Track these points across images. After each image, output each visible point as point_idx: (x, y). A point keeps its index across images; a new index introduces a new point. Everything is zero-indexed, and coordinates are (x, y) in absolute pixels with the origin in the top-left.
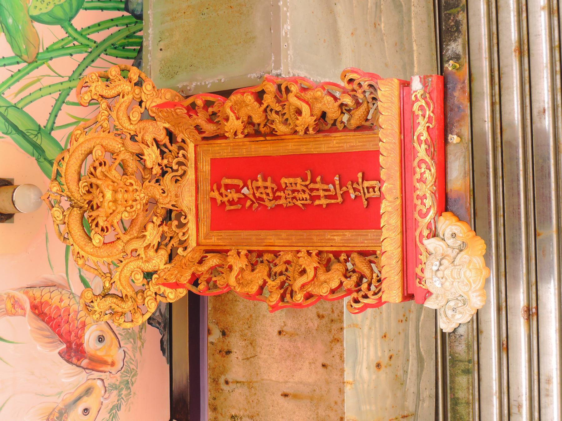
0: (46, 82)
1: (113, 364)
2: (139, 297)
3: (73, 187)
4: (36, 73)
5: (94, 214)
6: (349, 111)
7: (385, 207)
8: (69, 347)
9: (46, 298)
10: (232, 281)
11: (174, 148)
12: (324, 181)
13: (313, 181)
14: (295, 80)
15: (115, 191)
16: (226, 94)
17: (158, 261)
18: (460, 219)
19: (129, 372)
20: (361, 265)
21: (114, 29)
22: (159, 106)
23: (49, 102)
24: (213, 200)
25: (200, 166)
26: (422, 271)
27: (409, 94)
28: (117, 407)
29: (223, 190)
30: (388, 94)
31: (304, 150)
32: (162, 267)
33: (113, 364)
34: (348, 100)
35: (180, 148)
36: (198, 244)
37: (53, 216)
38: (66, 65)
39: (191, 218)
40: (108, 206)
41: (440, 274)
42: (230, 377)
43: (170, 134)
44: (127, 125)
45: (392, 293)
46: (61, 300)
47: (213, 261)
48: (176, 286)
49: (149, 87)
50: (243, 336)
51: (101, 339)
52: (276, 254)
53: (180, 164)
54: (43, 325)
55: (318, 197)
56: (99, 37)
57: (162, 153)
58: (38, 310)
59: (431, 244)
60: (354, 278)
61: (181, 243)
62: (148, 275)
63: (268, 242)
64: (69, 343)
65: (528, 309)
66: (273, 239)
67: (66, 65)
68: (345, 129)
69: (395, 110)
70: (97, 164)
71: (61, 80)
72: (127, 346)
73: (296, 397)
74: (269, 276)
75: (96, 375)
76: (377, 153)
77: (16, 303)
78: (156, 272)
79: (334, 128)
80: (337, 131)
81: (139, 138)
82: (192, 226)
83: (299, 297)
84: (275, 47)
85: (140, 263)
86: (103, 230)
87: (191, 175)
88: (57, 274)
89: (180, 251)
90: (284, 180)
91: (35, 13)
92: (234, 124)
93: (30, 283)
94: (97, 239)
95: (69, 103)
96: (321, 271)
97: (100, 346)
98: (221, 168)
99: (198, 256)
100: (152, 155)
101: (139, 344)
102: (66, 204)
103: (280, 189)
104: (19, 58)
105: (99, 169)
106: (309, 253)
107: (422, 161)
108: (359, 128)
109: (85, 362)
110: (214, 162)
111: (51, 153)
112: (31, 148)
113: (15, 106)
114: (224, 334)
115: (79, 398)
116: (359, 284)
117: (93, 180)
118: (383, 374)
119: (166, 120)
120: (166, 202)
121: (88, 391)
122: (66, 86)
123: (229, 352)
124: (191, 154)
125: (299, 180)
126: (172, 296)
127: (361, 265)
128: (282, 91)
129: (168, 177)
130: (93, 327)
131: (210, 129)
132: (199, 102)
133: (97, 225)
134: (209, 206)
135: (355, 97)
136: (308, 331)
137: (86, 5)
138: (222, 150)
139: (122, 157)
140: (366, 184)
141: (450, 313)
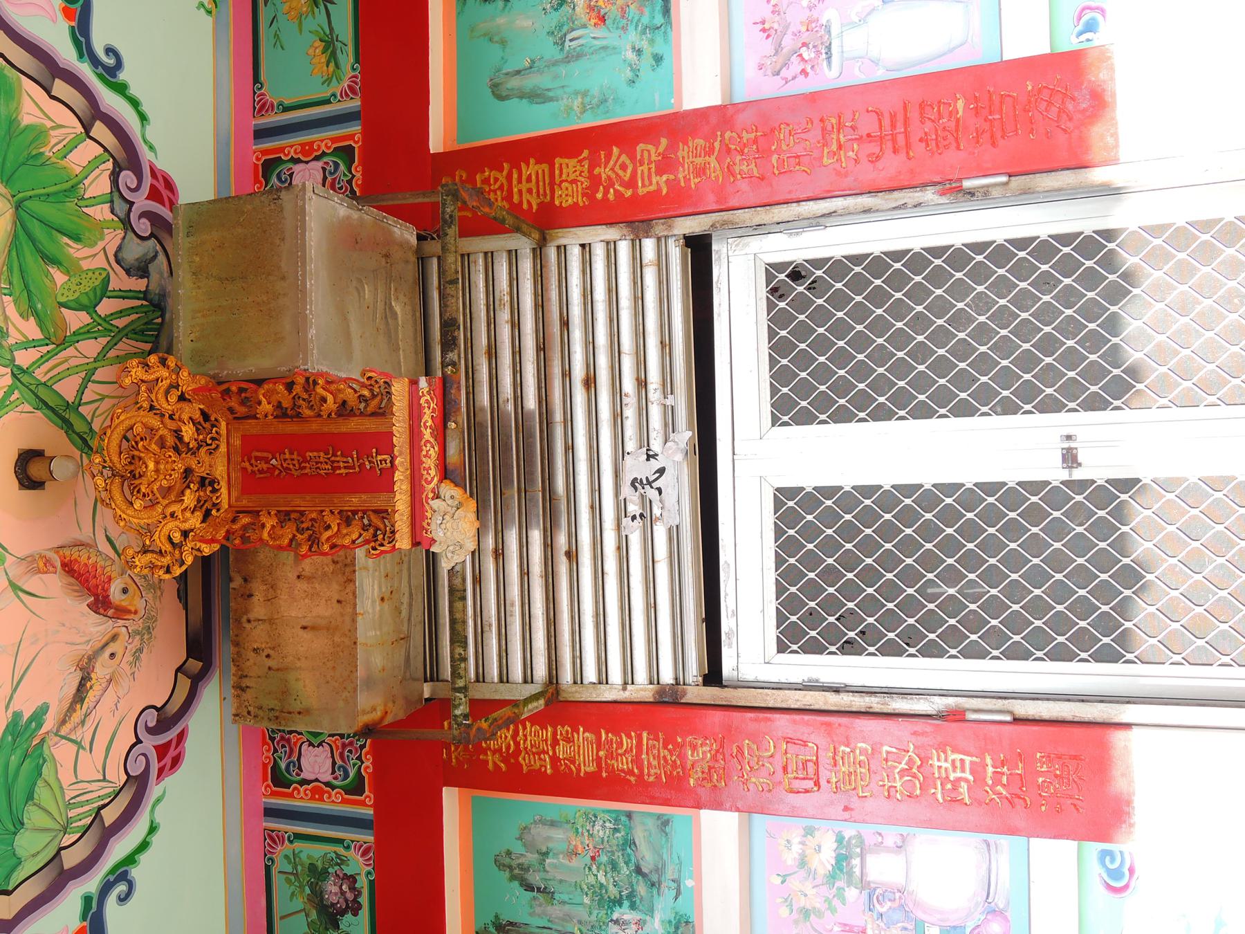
0: (73, 362)
1: (136, 612)
2: (177, 552)
3: (115, 459)
4: (63, 354)
5: (137, 482)
6: (366, 401)
7: (398, 476)
8: (96, 600)
9: (75, 556)
10: (265, 536)
11: (207, 425)
12: (342, 455)
13: (334, 455)
14: (321, 374)
15: (157, 463)
16: (259, 382)
17: (195, 521)
18: (456, 485)
19: (150, 619)
20: (376, 521)
21: (134, 317)
22: (194, 390)
23: (74, 382)
24: (244, 469)
25: (232, 441)
26: (428, 524)
27: (417, 390)
28: (140, 650)
29: (253, 461)
30: (399, 389)
31: (326, 429)
32: (198, 526)
33: (136, 612)
34: (366, 393)
35: (213, 426)
36: (230, 506)
37: (95, 484)
38: (91, 347)
39: (224, 484)
40: (151, 474)
41: (443, 526)
42: (252, 616)
43: (203, 413)
44: (165, 405)
45: (403, 542)
46: (89, 558)
47: (246, 520)
48: (213, 541)
49: (186, 374)
50: (264, 582)
51: (125, 591)
52: (302, 513)
53: (212, 439)
54: (72, 580)
55: (339, 468)
56: (121, 323)
57: (197, 430)
58: (69, 568)
59: (436, 504)
60: (371, 531)
61: (214, 505)
62: (185, 534)
63: (293, 503)
64: (96, 596)
65: (496, 551)
66: (299, 502)
67: (91, 347)
68: (362, 414)
69: (406, 403)
70: (138, 438)
71: (87, 361)
72: (149, 596)
73: (314, 628)
74: (298, 530)
75: (121, 622)
76: (391, 434)
77: (48, 562)
78: (192, 530)
79: (352, 413)
80: (355, 415)
81: (176, 417)
82: (224, 491)
83: (326, 547)
84: (302, 346)
85: (177, 523)
86: (144, 495)
87: (223, 449)
88: (85, 534)
89: (214, 512)
90: (309, 454)
91: (62, 299)
92: (266, 407)
93: (60, 544)
94: (138, 504)
95: (94, 382)
96: (342, 526)
97: (124, 597)
98: (250, 445)
99: (230, 516)
100: (188, 432)
101: (159, 593)
102: (107, 473)
103: (305, 461)
104: (48, 340)
105: (141, 444)
106: (332, 512)
107: (428, 441)
108: (373, 414)
109: (110, 613)
110: (244, 438)
111: (79, 426)
112: (60, 422)
113: (45, 384)
114: (246, 580)
115: (106, 644)
116: (375, 535)
117: (136, 453)
118: (386, 605)
119: (201, 402)
120: (201, 471)
121: (114, 638)
122: (91, 366)
123: (251, 596)
124: (223, 431)
125: (322, 454)
126: (207, 550)
127: (376, 521)
128: (310, 383)
129: (203, 450)
130: (119, 581)
131: (242, 410)
132: (234, 388)
133: (138, 492)
134: (239, 474)
135: (371, 391)
136: (325, 574)
137: (109, 294)
138: (252, 427)
139: (161, 432)
140: (379, 458)
141: (449, 555)
